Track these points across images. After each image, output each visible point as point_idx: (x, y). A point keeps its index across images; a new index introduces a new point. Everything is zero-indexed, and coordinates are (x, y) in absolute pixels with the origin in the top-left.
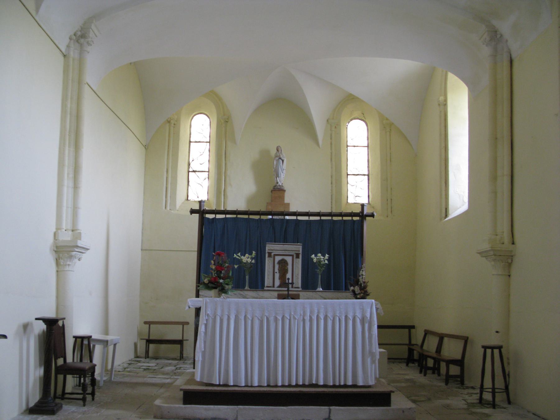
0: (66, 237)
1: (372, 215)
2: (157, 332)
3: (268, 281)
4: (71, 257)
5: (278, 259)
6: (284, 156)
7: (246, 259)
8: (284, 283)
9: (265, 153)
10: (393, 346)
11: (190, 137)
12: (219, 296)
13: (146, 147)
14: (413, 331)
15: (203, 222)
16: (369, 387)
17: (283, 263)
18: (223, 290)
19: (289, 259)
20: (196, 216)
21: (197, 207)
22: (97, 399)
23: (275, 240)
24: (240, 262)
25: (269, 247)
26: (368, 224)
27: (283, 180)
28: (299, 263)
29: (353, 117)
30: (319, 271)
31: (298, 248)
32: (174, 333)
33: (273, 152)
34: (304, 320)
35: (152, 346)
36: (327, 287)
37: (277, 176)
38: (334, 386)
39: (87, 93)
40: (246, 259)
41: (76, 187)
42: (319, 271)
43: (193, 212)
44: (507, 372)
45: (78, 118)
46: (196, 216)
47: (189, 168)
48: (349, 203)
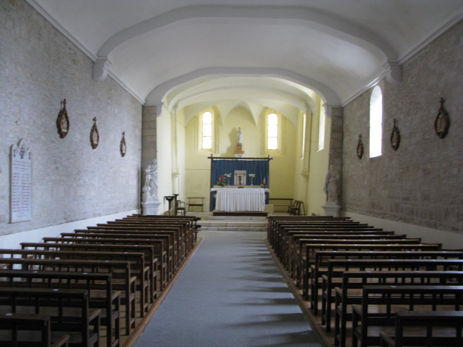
0: (175, 171)
1: (272, 159)
2: (193, 201)
3: (235, 183)
4: (176, 176)
5: (238, 175)
6: (242, 131)
7: (229, 176)
8: (240, 184)
9: (234, 130)
10: (282, 207)
11: (202, 122)
12: (222, 187)
13: (186, 127)
14: (271, 196)
15: (213, 162)
16: (262, 212)
17: (240, 177)
18: (223, 186)
19: (242, 176)
20: (210, 159)
21: (210, 156)
22: (33, 299)
23: (238, 169)
24: (226, 176)
25: (236, 172)
26: (271, 163)
27: (241, 141)
28: (245, 177)
29: (271, 112)
30: (252, 179)
31: (245, 172)
32: (199, 202)
33: (237, 130)
34: (244, 194)
35: (191, 207)
36: (254, 184)
37: (239, 139)
38: (252, 211)
39: (178, 123)
40: (229, 176)
41: (176, 155)
42: (252, 179)
43: (209, 158)
44: (305, 210)
45: (176, 133)
46: (210, 159)
47: (202, 135)
48: (277, 135)
